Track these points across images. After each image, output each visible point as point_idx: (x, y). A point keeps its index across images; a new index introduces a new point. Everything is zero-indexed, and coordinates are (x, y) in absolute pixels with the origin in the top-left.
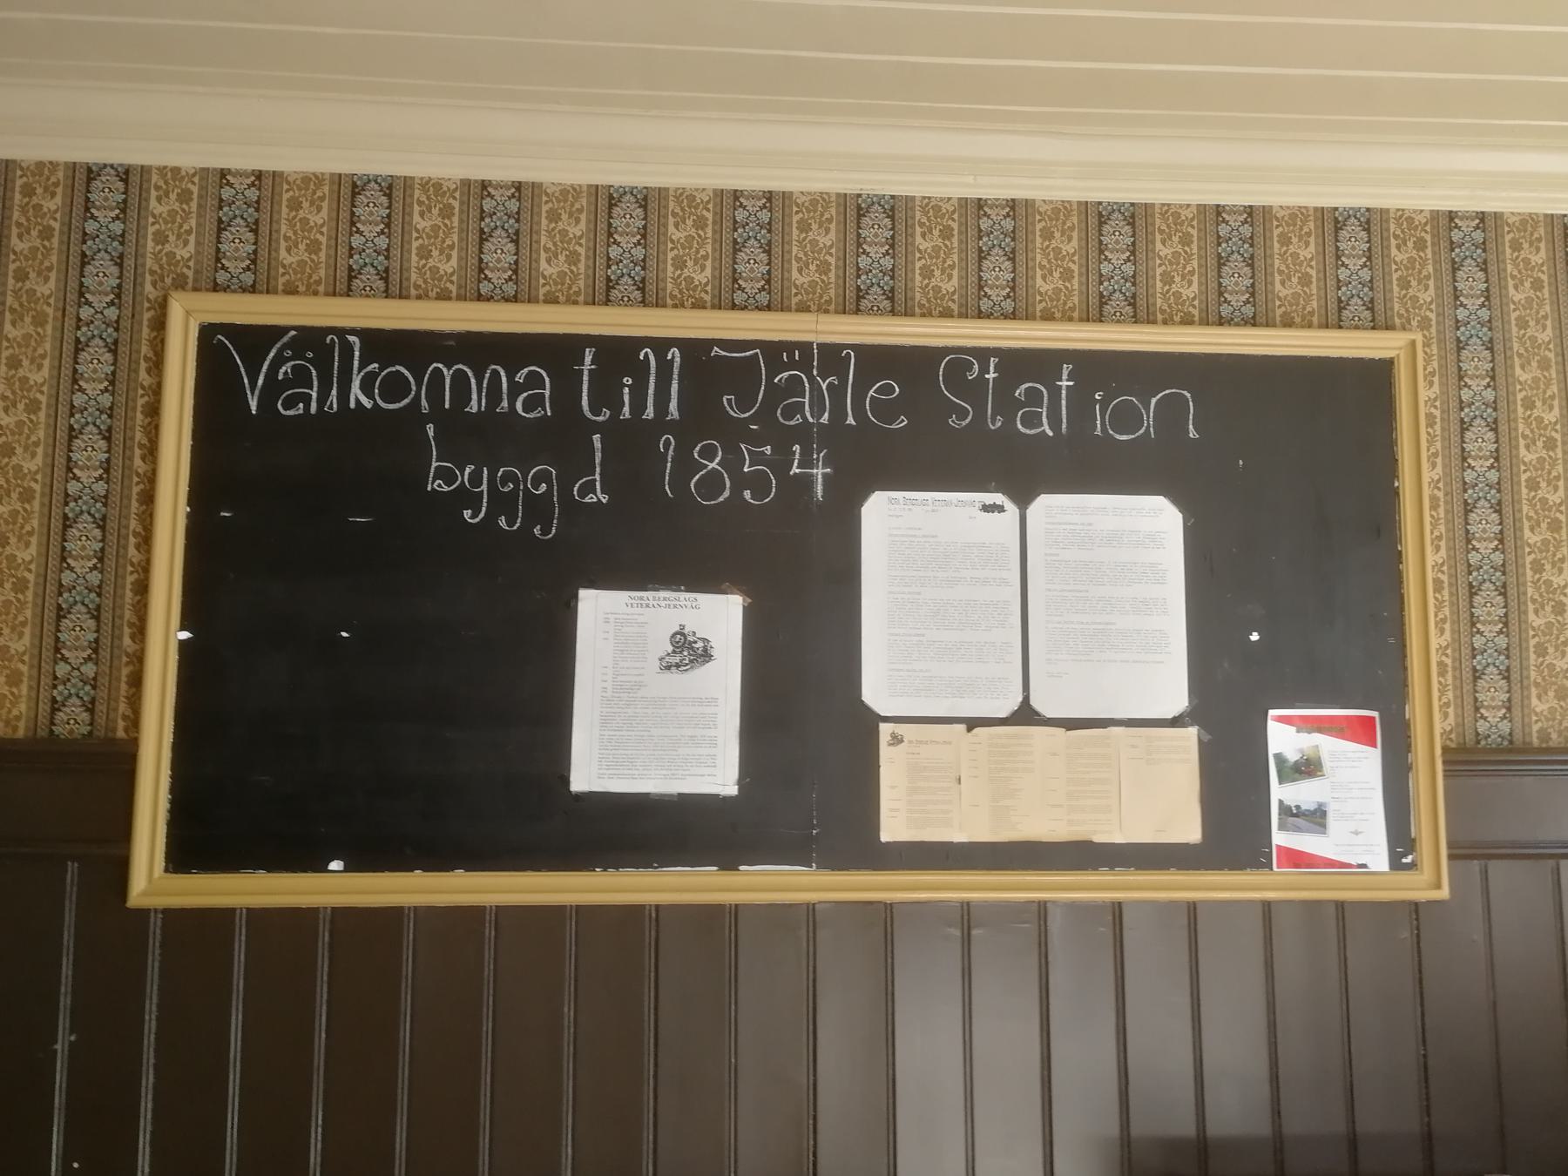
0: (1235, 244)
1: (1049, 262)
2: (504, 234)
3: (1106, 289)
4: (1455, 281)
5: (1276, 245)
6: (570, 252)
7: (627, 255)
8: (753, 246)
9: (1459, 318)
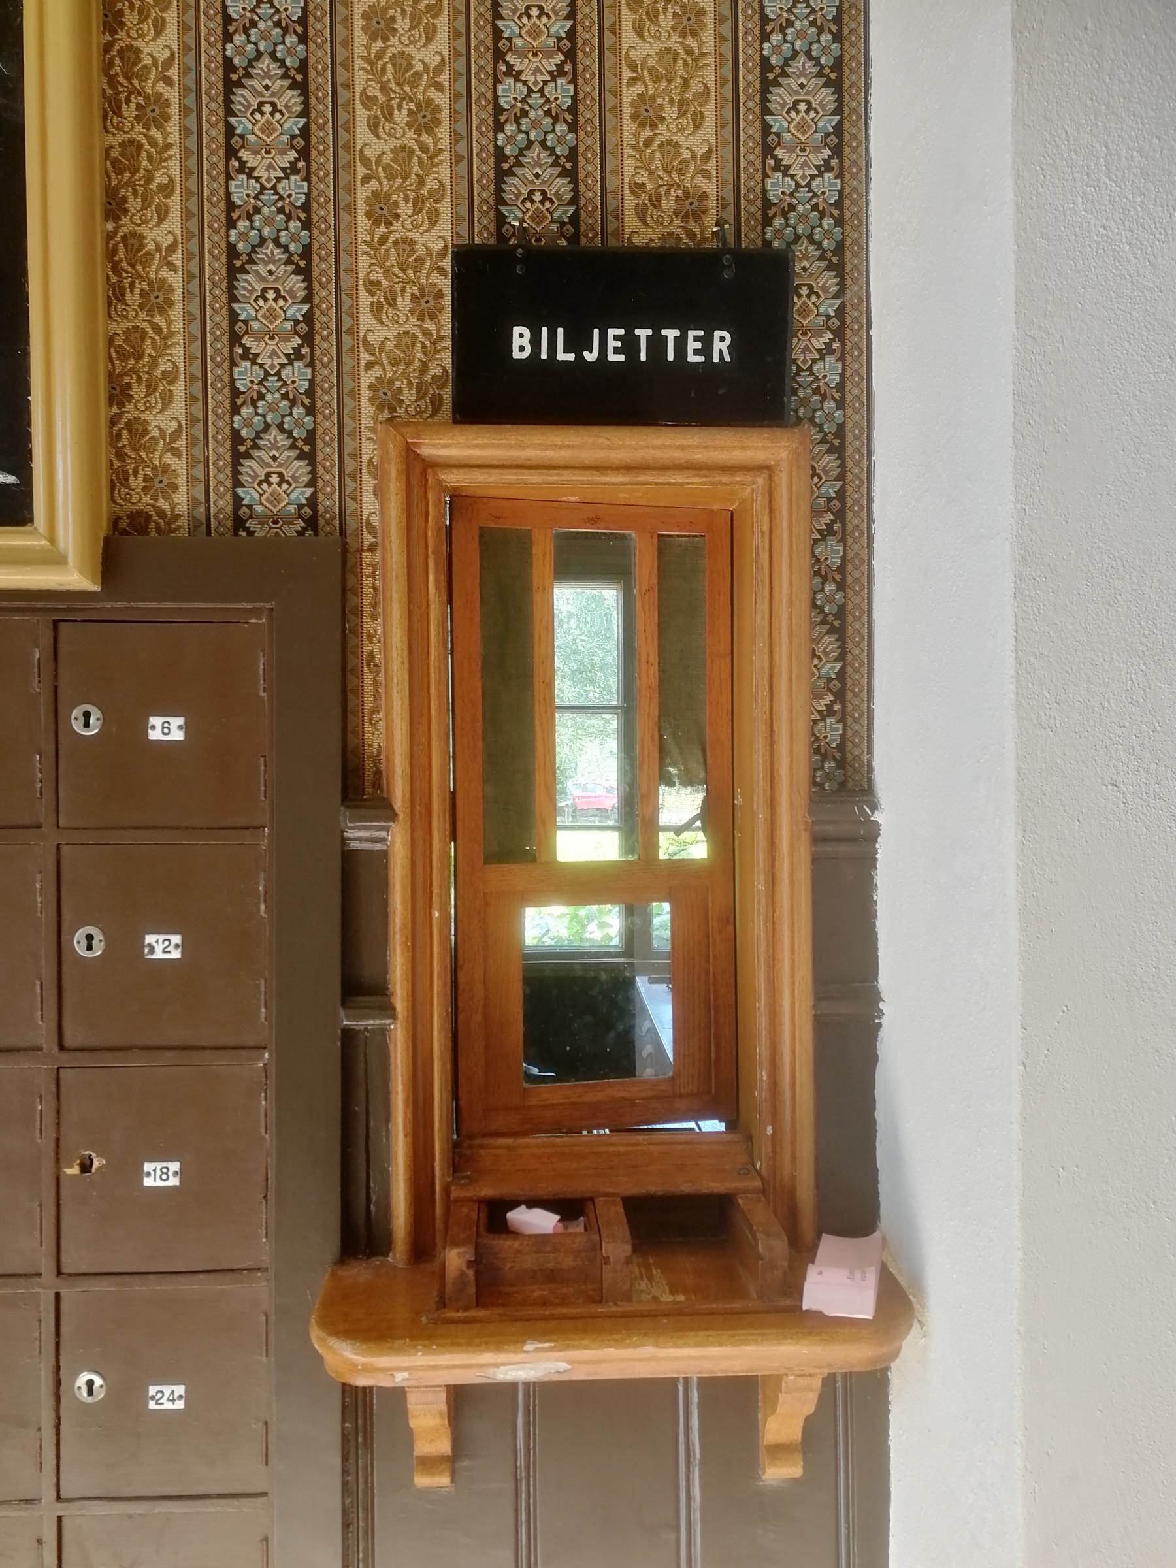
0: (264, 36)
1: (384, 88)
2: (275, 69)
3: (510, 139)
4: (230, 112)
5: (360, 37)
6: (418, 104)
7: (536, 99)
8: (267, 75)
9: (237, 199)
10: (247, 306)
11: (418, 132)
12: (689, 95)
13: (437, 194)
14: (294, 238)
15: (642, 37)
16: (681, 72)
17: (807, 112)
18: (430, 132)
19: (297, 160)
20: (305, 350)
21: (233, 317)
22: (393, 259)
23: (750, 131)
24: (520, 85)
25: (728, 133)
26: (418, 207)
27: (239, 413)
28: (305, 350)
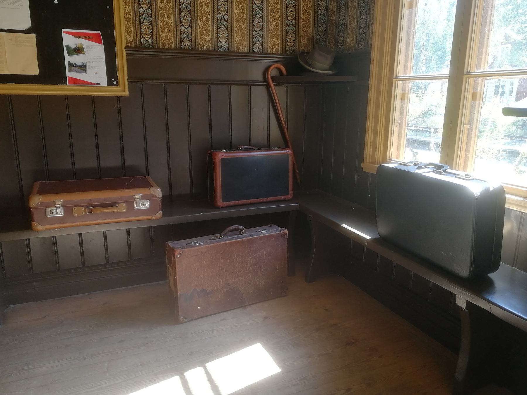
10: (143, 30)
11: (168, 3)
12: (169, 13)
13: (171, 14)
14: (189, 8)
15: (161, 3)
16: (167, 9)
17: (186, 17)
18: (169, 4)
19: (150, 6)
20: (190, 25)
21: (218, 7)
22: (202, 13)
23: (178, 20)
24: (143, 10)
25: (175, 19)
26: (168, 16)
27: (181, 35)
28: (190, 25)
